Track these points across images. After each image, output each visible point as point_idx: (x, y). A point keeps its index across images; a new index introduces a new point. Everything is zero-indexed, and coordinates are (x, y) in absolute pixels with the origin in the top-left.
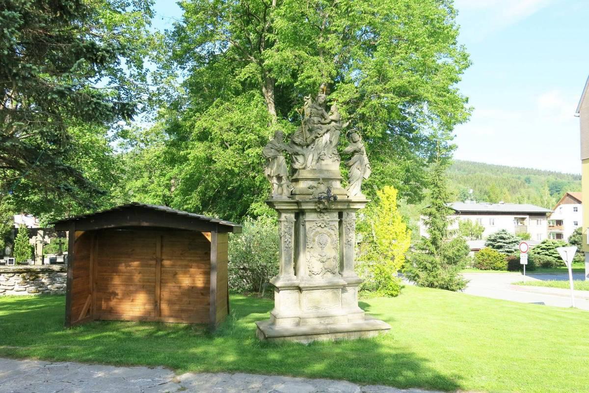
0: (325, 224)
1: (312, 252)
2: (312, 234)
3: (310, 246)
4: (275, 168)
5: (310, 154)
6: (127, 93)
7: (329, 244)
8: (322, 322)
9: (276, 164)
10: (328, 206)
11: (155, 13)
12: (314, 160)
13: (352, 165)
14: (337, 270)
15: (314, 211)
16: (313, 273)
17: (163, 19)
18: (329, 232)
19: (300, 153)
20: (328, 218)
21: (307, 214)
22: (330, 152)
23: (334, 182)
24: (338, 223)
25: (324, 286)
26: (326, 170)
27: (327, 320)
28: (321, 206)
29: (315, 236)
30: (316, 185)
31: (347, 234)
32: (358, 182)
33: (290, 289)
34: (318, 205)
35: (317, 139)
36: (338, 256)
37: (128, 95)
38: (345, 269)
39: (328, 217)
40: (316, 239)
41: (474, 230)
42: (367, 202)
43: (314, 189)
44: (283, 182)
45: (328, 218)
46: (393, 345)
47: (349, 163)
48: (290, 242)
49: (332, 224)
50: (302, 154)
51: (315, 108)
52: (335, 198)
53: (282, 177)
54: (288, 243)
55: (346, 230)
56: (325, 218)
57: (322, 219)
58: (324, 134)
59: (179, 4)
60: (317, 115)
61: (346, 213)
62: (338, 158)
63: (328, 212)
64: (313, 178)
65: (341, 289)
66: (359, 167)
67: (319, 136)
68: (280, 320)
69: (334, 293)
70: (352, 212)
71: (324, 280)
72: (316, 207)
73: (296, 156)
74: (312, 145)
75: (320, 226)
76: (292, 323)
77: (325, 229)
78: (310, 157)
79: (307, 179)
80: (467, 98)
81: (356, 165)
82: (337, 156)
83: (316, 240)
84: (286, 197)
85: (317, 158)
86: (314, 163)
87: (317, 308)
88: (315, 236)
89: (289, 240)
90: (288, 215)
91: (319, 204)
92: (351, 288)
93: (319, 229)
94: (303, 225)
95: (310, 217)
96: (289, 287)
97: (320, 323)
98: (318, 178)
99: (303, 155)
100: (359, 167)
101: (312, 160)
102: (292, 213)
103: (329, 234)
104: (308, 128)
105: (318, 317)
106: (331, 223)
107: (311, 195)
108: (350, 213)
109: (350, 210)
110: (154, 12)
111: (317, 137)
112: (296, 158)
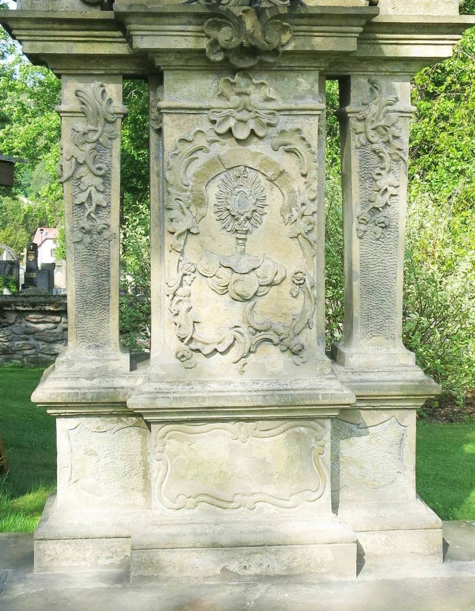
0: (252, 125)
1: (191, 256)
2: (194, 167)
3: (181, 227)
7: (272, 216)
8: (234, 567)
14: (311, 338)
16: (193, 346)
18: (273, 164)
20: (269, 100)
25: (248, 409)
28: (224, 35)
29: (204, 176)
31: (369, 178)
33: (99, 415)
34: (214, 33)
36: (315, 273)
38: (358, 332)
39: (270, 92)
40: (213, 192)
41: (36, 210)
45: (269, 100)
49: (289, 127)
54: (91, 209)
55: (364, 158)
56: (256, 97)
57: (235, 100)
61: (364, 81)
63: (263, 68)
68: (43, 545)
69: (299, 437)
70: (393, 74)
71: (246, 379)
72: (204, 44)
75: (230, 132)
76: (102, 561)
77: (255, 147)
87: (217, 502)
88: (204, 176)
90: (91, 88)
91: (218, 26)
92: (385, 415)
93: (225, 148)
96: (89, 404)
97: (224, 570)
102: (108, 76)
105: (215, 546)
106: (284, 122)
108: (382, 83)
109: (389, 67)
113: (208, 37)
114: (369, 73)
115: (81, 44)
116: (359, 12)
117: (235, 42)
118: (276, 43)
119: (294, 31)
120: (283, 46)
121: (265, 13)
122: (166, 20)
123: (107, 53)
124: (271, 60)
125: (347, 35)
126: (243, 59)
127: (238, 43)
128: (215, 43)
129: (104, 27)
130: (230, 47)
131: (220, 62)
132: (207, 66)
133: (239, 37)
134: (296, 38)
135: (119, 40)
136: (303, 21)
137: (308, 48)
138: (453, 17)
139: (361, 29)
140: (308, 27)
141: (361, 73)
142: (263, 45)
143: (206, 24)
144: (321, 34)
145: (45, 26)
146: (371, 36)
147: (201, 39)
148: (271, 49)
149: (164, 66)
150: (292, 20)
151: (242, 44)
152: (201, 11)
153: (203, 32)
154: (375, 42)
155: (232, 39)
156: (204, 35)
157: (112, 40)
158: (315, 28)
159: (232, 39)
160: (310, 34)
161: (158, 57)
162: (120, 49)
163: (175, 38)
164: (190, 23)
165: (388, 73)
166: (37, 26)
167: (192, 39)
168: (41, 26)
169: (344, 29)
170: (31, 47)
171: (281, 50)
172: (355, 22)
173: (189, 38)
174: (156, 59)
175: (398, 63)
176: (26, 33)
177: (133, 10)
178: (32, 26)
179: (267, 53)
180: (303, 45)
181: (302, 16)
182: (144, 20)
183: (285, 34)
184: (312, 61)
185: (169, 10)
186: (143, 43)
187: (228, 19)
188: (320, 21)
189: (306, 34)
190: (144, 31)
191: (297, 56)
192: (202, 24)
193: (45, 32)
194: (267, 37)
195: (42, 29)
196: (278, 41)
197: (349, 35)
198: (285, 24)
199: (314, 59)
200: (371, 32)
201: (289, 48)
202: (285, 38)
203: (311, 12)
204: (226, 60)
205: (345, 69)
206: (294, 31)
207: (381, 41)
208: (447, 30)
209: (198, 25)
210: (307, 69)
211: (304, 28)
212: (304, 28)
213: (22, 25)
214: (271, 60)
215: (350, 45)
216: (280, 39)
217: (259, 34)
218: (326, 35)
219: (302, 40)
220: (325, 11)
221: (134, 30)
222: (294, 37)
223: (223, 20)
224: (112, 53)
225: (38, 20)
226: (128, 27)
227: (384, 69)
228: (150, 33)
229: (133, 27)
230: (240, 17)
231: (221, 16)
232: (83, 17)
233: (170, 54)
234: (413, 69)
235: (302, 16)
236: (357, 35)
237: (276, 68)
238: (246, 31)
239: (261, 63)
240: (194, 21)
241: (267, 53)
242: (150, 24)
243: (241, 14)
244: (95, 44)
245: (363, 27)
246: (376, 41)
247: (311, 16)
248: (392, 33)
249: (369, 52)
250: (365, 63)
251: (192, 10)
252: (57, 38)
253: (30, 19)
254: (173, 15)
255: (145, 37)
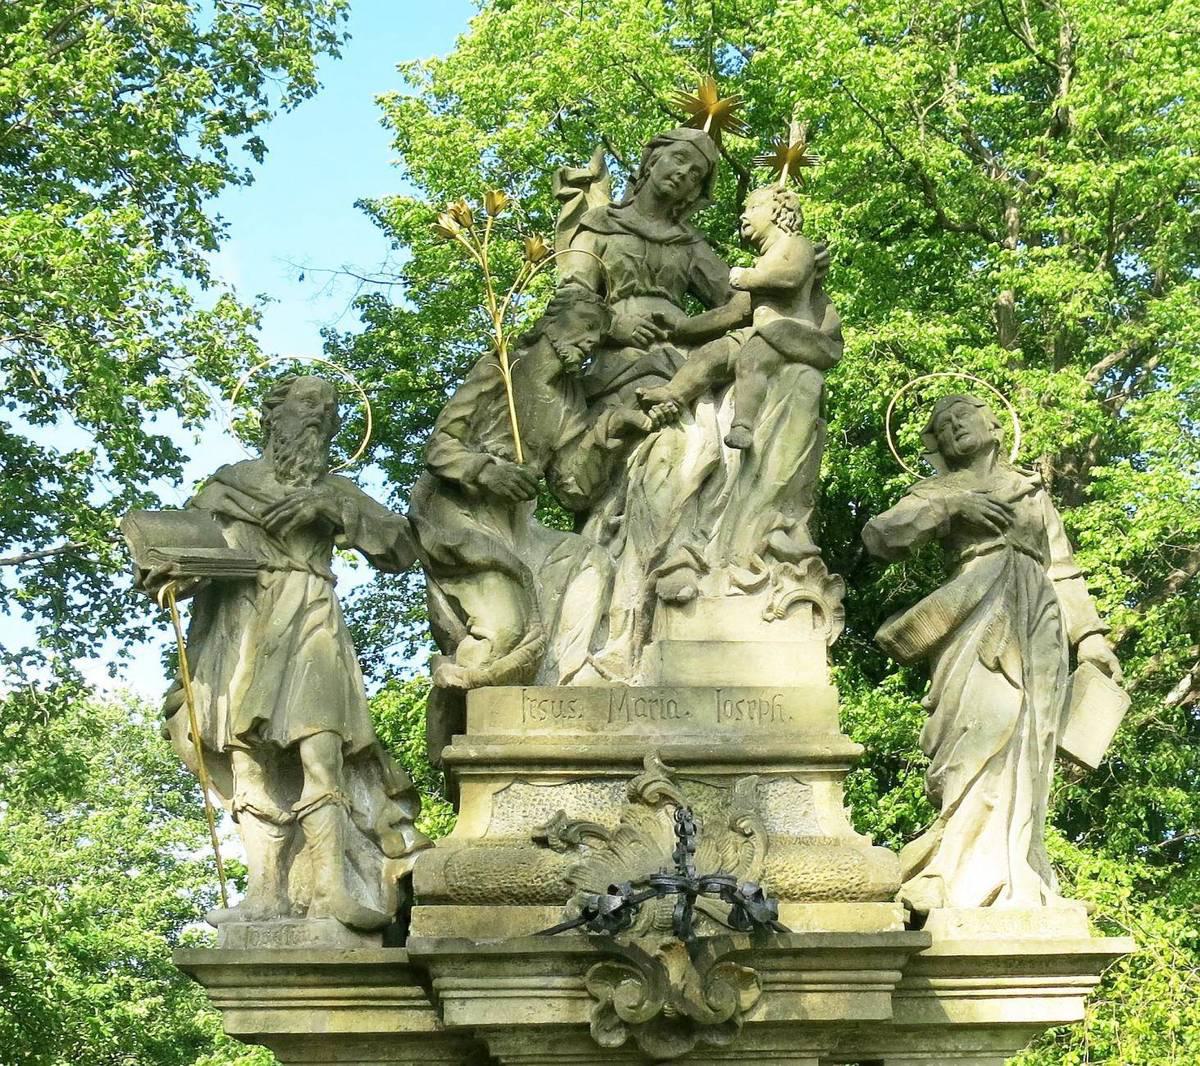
4: (237, 679)
5: (575, 570)
6: (96, 583)
9: (245, 639)
10: (694, 992)
11: (226, 230)
12: (615, 622)
13: (943, 642)
17: (302, 278)
19: (474, 555)
22: (747, 544)
23: (783, 787)
26: (700, 690)
28: (626, 995)
30: (609, 819)
32: (1001, 782)
34: (605, 991)
35: (639, 449)
37: (96, 596)
42: (1105, 959)
43: (590, 849)
44: (311, 791)
47: (909, 627)
50: (495, 567)
51: (629, 230)
52: (765, 928)
53: (296, 746)
58: (691, 404)
59: (366, 206)
60: (650, 280)
62: (814, 590)
64: (582, 750)
66: (998, 648)
67: (648, 424)
72: (586, 1013)
73: (450, 588)
74: (609, 506)
78: (582, 597)
79: (527, 767)
81: (974, 634)
82: (801, 569)
84: (333, 926)
85: (636, 603)
86: (619, 643)
91: (614, 977)
98: (629, 751)
99: (515, 575)
100: (998, 648)
101: (604, 618)
104: (553, 365)
107: (556, 899)
109: (962, 1043)
110: (218, 225)
111: (631, 434)
112: (453, 601)
113: (596, 999)
114: (919, 1055)
115: (341, 1014)
116: (891, 943)
117: (649, 1009)
118: (729, 1010)
119: (765, 983)
120: (744, 1013)
121: (705, 950)
122: (510, 967)
123: (393, 1029)
124: (721, 1042)
125: (870, 987)
126: (666, 1040)
127: (654, 1011)
128: (608, 1010)
129: (389, 978)
130: (638, 1020)
131: (620, 1047)
132: (593, 1055)
133: (655, 999)
134: (770, 995)
135: (417, 1003)
136: (784, 962)
137: (795, 1017)
138: (1079, 942)
139: (897, 975)
140: (793, 974)
141: (906, 1056)
142: (705, 1013)
143: (589, 974)
144: (819, 987)
145: (272, 979)
146: (919, 982)
147: (579, 1003)
148: (720, 1021)
149: (507, 1057)
150: (760, 962)
151: (661, 1013)
152: (581, 948)
153: (584, 989)
154: (928, 995)
155: (641, 1003)
156: (585, 994)
157: (403, 1003)
158: (805, 976)
159: (641, 1003)
160: (797, 988)
161: (495, 1039)
162: (417, 1021)
163: (528, 1003)
164: (557, 973)
165: (959, 1055)
166: (254, 980)
167: (563, 1004)
168: (262, 979)
169: (864, 975)
170: (242, 1022)
171: (740, 1020)
172: (885, 961)
173: (557, 1001)
174: (491, 1044)
175: (978, 1033)
176: (233, 993)
177: (446, 950)
178: (245, 979)
179: (714, 1028)
180: (785, 1011)
181: (779, 954)
182: (466, 968)
183: (747, 989)
184: (804, 1040)
185: (516, 948)
186: (465, 1014)
187: (633, 964)
188: (815, 962)
189: (789, 987)
190: (466, 989)
191: (774, 1031)
192: (582, 973)
193: (270, 992)
194: (712, 999)
195: (265, 986)
196: (733, 1005)
197: (875, 987)
198: (747, 969)
199: (808, 1035)
200: (917, 975)
201: (758, 1016)
202: (748, 996)
203: (796, 945)
204: (631, 1042)
205: (873, 1049)
206: (765, 983)
207: (939, 993)
208: (1070, 967)
209: (573, 975)
210: (796, 1055)
211: (786, 976)
212: (786, 976)
213: (225, 979)
214: (721, 1042)
215: (879, 1007)
216: (738, 999)
217: (694, 992)
218: (831, 988)
219: (783, 999)
220: (825, 944)
221: (446, 989)
222: (765, 994)
223: (622, 966)
224: (402, 1029)
225: (257, 969)
226: (436, 983)
227: (949, 1047)
228: (477, 994)
229: (445, 982)
230: (658, 958)
231: (620, 958)
232: (347, 961)
233: (518, 1033)
234: (1008, 1043)
235: (779, 954)
236: (892, 987)
237: (731, 1056)
238: (670, 988)
239: (702, 1047)
240: (567, 968)
241: (714, 1028)
242: (480, 976)
243: (658, 952)
244: (369, 1012)
245: (900, 969)
246: (930, 993)
247: (798, 953)
248: (961, 976)
249: (916, 1013)
250: (910, 1035)
251: (562, 948)
252: (293, 1003)
253: (242, 968)
254: (525, 957)
255: (468, 1003)
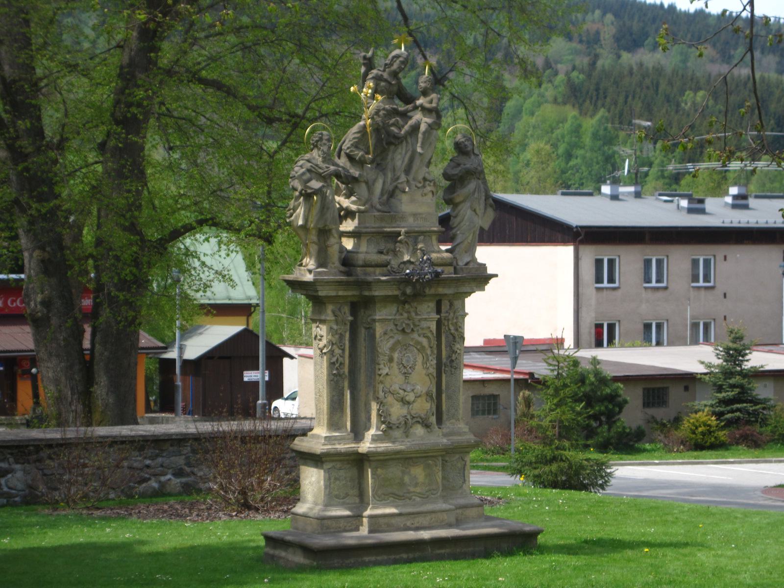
14: (433, 419)
15: (393, 299)
21: (378, 305)
24: (435, 323)
27: (417, 520)
46: (445, 441)
48: (341, 364)
65: (440, 459)
80: (665, 51)
83: (396, 360)
89: (341, 359)
94: (366, 328)
95: (383, 313)
103: (418, 347)
